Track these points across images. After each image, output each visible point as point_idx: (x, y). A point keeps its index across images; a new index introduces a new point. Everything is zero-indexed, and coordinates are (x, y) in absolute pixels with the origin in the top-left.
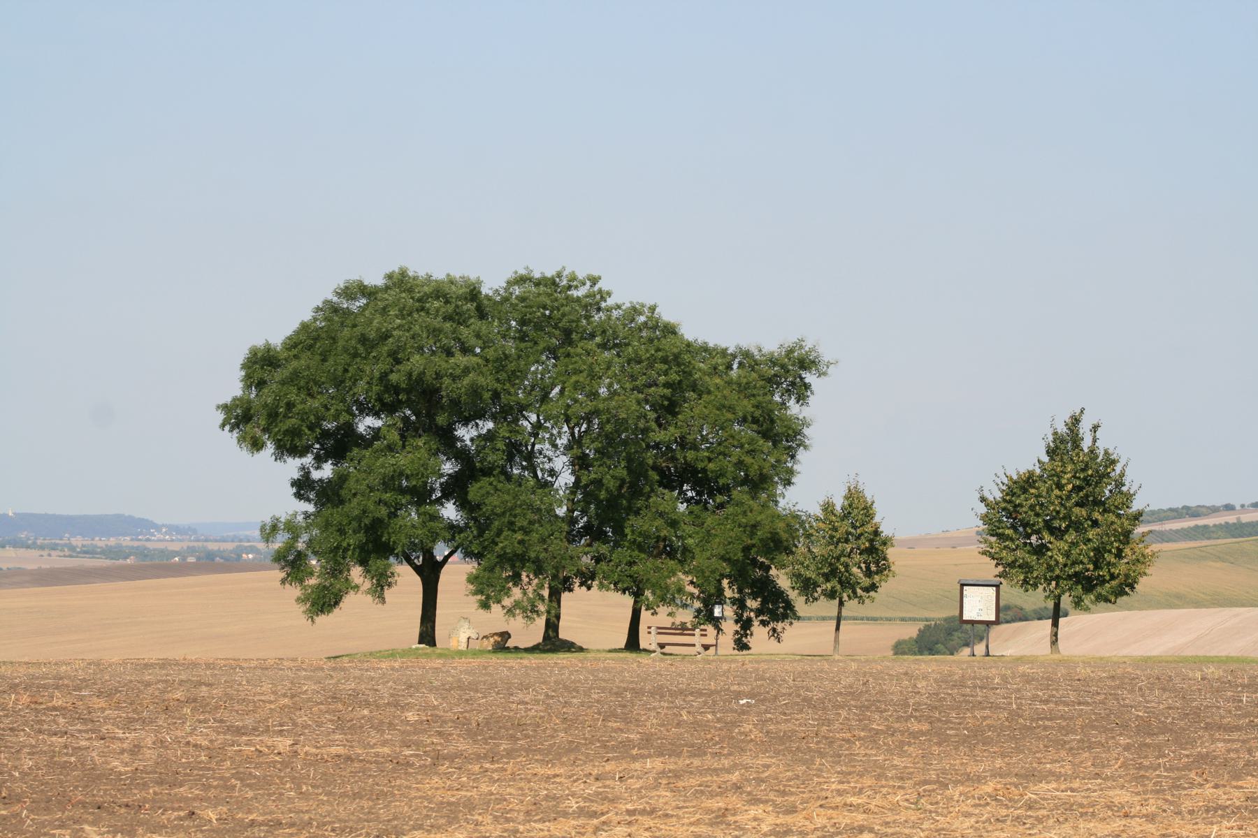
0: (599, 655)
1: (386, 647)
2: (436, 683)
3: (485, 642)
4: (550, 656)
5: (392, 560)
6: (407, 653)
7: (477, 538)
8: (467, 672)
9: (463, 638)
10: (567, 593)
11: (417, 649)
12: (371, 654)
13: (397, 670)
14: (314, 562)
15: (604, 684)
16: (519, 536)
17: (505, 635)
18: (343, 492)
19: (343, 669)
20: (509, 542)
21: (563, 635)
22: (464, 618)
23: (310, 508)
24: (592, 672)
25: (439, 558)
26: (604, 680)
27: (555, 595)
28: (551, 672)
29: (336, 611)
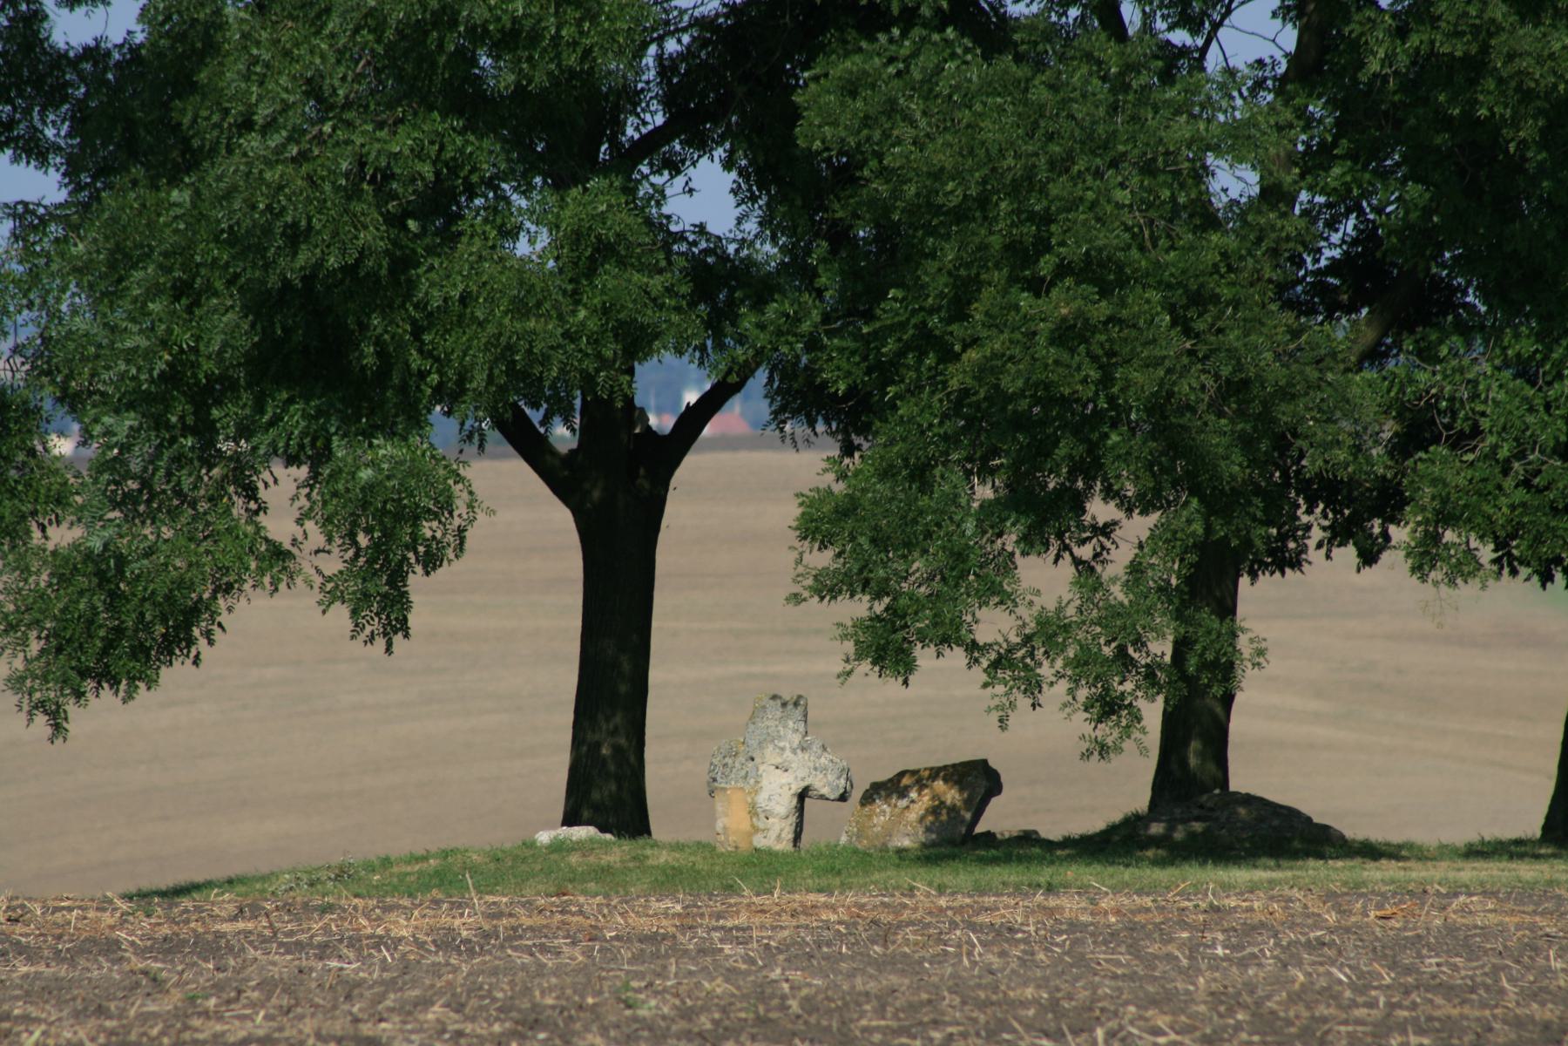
0: (1417, 872)
1: (401, 844)
2: (649, 1007)
3: (883, 811)
4: (1213, 876)
5: (442, 428)
6: (513, 866)
7: (851, 325)
8: (796, 954)
9: (776, 791)
10: (1269, 583)
11: (558, 847)
12: (342, 874)
13: (469, 949)
14: (63, 446)
15: (1446, 1009)
16: (1062, 303)
17: (980, 780)
18: (185, 113)
19: (213, 947)
20: (1015, 335)
21: (1248, 774)
22: (775, 713)
23: (45, 186)
24: (1388, 952)
25: (661, 422)
26: (1448, 990)
27: (1208, 584)
28: (1193, 949)
29: (175, 674)
